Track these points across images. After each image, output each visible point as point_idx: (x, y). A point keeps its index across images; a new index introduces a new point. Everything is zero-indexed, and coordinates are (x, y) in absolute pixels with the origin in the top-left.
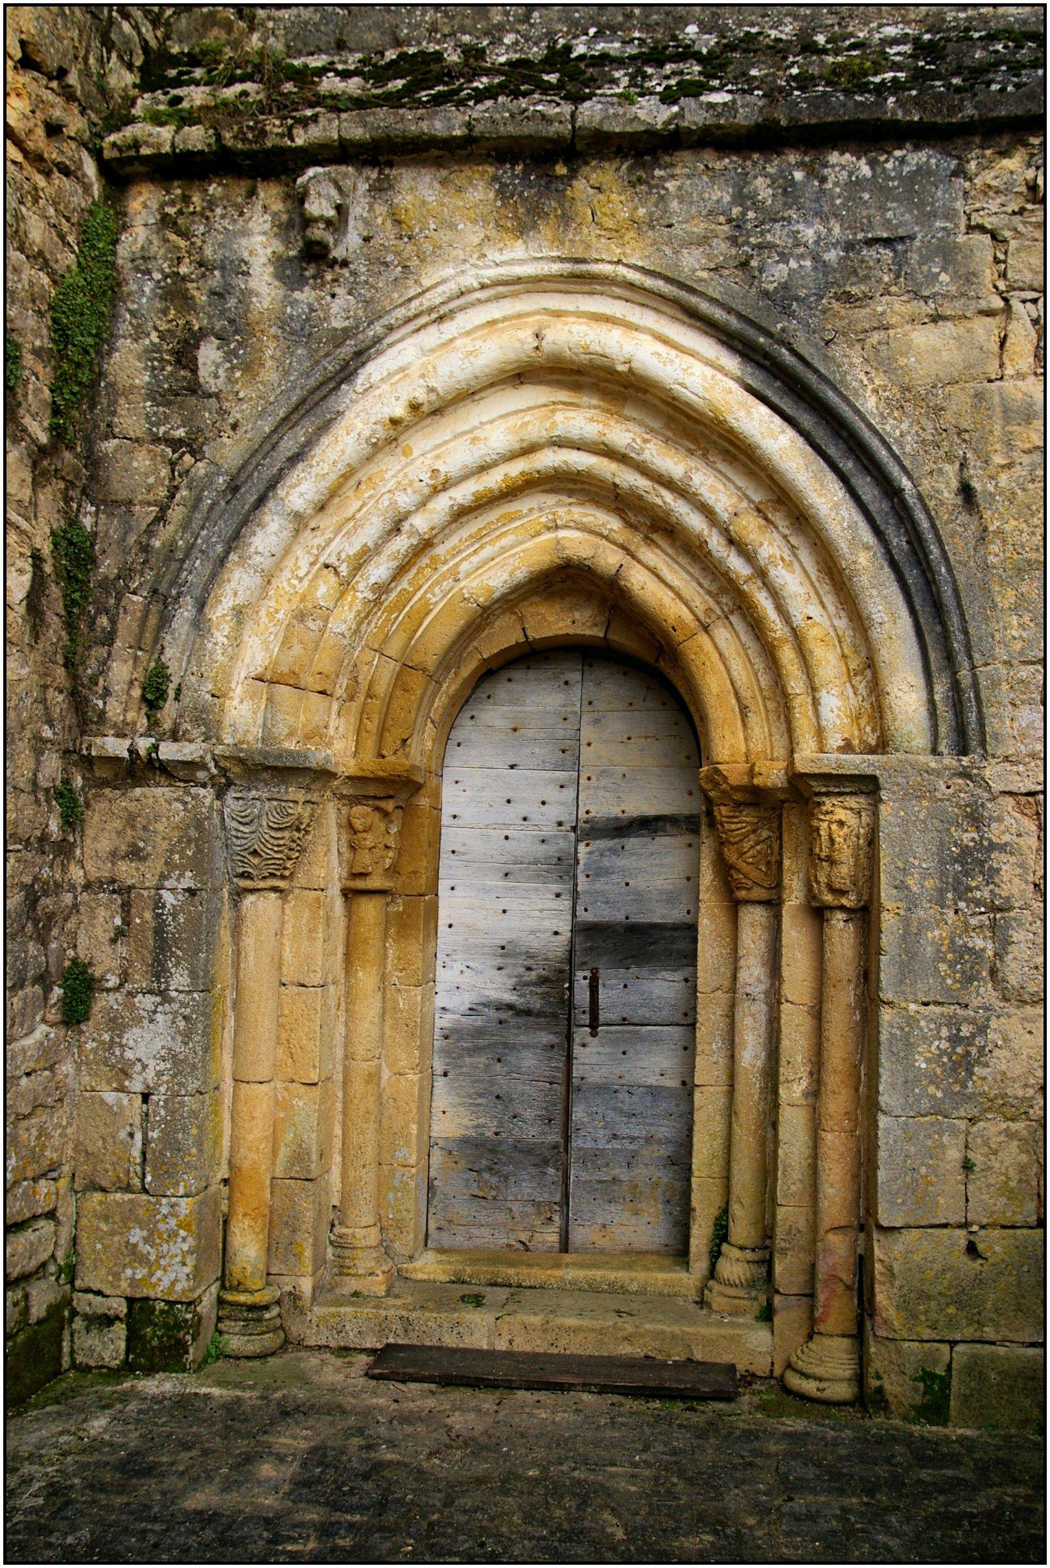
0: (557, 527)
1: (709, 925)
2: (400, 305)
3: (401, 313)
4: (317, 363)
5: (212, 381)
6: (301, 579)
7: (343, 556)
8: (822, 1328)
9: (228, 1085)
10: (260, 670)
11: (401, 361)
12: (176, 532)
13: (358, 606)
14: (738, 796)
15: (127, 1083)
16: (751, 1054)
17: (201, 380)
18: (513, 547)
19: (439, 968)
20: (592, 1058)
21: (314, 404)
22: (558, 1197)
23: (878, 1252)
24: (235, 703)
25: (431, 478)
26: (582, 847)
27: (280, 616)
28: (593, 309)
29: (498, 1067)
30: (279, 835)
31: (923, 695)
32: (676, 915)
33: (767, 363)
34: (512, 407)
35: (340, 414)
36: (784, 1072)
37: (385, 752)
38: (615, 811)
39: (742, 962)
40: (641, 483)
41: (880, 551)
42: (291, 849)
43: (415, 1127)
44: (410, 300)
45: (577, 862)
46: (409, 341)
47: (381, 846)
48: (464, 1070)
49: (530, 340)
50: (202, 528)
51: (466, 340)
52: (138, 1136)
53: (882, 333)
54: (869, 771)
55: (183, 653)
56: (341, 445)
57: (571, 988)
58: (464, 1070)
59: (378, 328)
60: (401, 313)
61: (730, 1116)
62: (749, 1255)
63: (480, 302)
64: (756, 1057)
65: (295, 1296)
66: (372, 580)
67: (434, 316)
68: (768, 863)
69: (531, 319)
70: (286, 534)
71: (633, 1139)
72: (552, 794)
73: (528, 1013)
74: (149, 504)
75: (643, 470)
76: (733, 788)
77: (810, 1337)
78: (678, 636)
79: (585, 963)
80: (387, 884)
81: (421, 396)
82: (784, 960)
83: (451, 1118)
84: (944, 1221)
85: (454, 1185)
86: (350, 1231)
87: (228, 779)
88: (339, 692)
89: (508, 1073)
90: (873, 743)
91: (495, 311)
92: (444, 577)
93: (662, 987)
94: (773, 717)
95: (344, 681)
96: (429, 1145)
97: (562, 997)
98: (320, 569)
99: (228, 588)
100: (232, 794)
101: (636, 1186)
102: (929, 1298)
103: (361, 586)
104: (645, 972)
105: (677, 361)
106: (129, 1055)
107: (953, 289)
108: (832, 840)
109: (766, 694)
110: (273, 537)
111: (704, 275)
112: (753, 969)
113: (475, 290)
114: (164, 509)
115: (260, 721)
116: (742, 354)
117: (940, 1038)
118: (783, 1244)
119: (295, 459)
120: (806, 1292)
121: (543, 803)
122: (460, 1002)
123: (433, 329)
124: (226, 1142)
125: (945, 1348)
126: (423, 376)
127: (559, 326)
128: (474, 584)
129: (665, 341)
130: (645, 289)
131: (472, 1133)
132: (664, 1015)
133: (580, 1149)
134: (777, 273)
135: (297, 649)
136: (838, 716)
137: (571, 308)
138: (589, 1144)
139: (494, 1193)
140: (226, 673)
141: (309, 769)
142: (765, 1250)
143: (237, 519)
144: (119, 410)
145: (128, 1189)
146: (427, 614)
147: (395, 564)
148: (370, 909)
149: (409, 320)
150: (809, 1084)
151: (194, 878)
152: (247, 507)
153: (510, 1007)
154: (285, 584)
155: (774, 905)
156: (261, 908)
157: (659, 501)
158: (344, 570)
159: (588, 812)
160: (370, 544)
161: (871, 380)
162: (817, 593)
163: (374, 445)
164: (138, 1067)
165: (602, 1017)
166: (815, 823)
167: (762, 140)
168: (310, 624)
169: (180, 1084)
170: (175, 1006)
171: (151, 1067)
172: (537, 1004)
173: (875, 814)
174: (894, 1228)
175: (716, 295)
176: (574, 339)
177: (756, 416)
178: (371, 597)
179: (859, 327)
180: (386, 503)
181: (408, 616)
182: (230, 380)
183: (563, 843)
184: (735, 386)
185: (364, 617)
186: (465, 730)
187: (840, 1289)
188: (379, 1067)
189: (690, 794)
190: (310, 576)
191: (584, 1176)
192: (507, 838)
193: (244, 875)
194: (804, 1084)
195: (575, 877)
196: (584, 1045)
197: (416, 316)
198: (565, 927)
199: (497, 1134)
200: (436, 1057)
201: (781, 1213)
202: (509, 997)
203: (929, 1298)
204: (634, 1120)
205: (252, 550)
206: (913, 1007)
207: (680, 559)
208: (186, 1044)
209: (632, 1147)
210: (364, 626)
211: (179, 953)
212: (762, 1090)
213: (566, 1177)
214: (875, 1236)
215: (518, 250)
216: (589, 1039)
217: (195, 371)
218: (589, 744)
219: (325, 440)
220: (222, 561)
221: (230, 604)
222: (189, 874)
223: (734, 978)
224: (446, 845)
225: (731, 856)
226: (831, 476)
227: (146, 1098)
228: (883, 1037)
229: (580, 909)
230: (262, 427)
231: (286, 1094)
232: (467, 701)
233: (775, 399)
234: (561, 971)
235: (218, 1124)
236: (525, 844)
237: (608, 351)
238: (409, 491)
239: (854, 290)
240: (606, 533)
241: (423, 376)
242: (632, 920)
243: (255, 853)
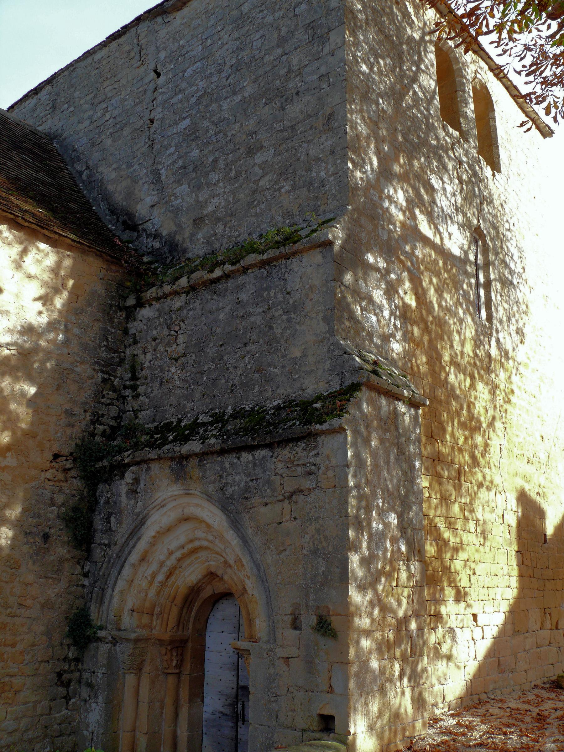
56: (142, 545)
59: (146, 512)
73: (226, 715)
100: (118, 645)
106: (90, 721)
111: (213, 493)
134: (230, 490)
153: (222, 712)
158: (149, 578)
167: (222, 452)
182: (117, 527)
198: (235, 687)
202: (221, 709)
215: (175, 487)
239: (247, 496)
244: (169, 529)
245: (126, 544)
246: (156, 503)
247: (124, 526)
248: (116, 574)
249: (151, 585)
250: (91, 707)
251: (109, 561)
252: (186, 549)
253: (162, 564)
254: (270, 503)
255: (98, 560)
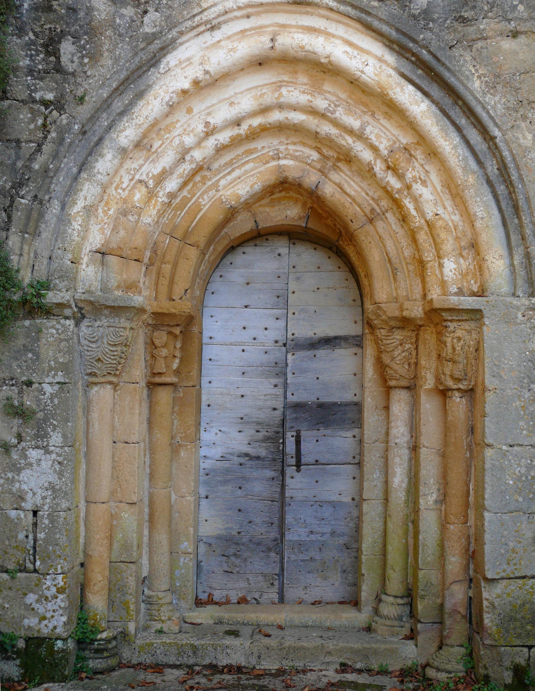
0: (279, 158)
1: (371, 401)
2: (189, 19)
3: (189, 23)
4: (136, 54)
5: (70, 64)
6: (124, 190)
7: (151, 175)
8: (448, 641)
9: (82, 505)
10: (99, 246)
11: (187, 55)
12: (48, 159)
13: (159, 207)
14: (393, 323)
15: (23, 504)
16: (399, 479)
17: (63, 64)
18: (252, 170)
19: (202, 432)
20: (297, 484)
21: (134, 80)
22: (277, 571)
23: (485, 595)
24: (84, 266)
25: (205, 127)
26: (289, 356)
27: (111, 212)
28: (306, 24)
29: (239, 492)
30: (114, 349)
31: (507, 261)
32: (348, 397)
33: (413, 59)
34: (255, 84)
35: (150, 87)
36: (422, 489)
37: (174, 298)
38: (310, 334)
39: (393, 424)
40: (333, 131)
41: (480, 172)
42: (121, 358)
43: (192, 529)
44: (194, 16)
45: (287, 365)
46: (192, 42)
47: (171, 356)
48: (218, 494)
49: (268, 42)
50: (65, 158)
51: (228, 42)
52: (31, 537)
53: (483, 42)
54: (477, 307)
55: (52, 235)
56: (151, 107)
57: (283, 443)
58: (218, 494)
59: (174, 33)
60: (189, 23)
61: (386, 518)
62: (400, 601)
63: (237, 18)
64: (402, 481)
65: (124, 634)
66: (168, 190)
67: (209, 26)
68: (409, 364)
69: (269, 29)
70: (116, 161)
71: (323, 534)
72: (271, 323)
73: (258, 458)
74: (31, 141)
75: (335, 123)
76: (389, 318)
77: (440, 648)
78: (354, 226)
79: (292, 427)
80: (174, 380)
81: (200, 75)
82: (422, 422)
83: (212, 523)
84: (523, 575)
85: (213, 563)
86: (155, 593)
87: (82, 314)
88: (146, 260)
89: (246, 495)
90: (476, 290)
91: (245, 24)
92: (209, 189)
93: (342, 441)
94: (412, 275)
95: (148, 254)
96: (198, 540)
97: (278, 448)
98: (136, 183)
99: (82, 194)
100: (85, 323)
101: (325, 563)
102: (516, 620)
103: (161, 194)
104: (328, 432)
105: (359, 57)
106: (24, 487)
107: (526, 15)
108: (454, 349)
109: (408, 261)
110: (109, 164)
112: (400, 428)
113: (234, 10)
114: (40, 146)
115: (99, 278)
116: (398, 53)
117: (521, 467)
118: (423, 593)
119: (122, 114)
120: (438, 620)
121: (266, 329)
122: (216, 452)
123: (207, 34)
124: (82, 540)
125: (526, 650)
126: (201, 64)
127: (286, 34)
128: (229, 193)
129: (350, 44)
130: (339, 13)
131: (223, 532)
132: (341, 458)
133: (290, 541)
135: (122, 233)
136: (455, 274)
137: (293, 23)
138: (296, 538)
139: (238, 569)
140: (79, 247)
141: (134, 307)
142: (410, 596)
143: (85, 152)
144: (10, 81)
145: (24, 570)
146: (199, 211)
147: (181, 180)
148: (164, 396)
149: (193, 28)
150: (438, 496)
151: (64, 376)
152: (92, 144)
153: (246, 455)
154: (114, 192)
155: (412, 388)
156: (102, 395)
157: (343, 142)
158: (151, 183)
159: (293, 334)
160: (167, 168)
161: (477, 71)
162: (442, 201)
163: (171, 106)
164: (30, 495)
165: (304, 460)
166: (444, 339)
168: (130, 217)
169: (57, 504)
170: (54, 456)
171: (39, 494)
172: (263, 453)
173: (480, 333)
174: (495, 579)
175: (383, 17)
176: (295, 43)
177: (406, 91)
178: (167, 201)
179: (469, 38)
180: (177, 142)
181: (187, 212)
182: (82, 64)
183: (278, 353)
184: (393, 73)
185: (161, 214)
186: (216, 284)
187: (459, 617)
188: (170, 492)
189: (356, 323)
190: (129, 188)
191: (293, 557)
192: (243, 351)
193: (94, 375)
194: (435, 496)
195: (285, 374)
196: (292, 478)
197: (198, 26)
198: (279, 404)
199: (239, 533)
200: (201, 486)
201: (421, 574)
203: (516, 620)
204: (323, 522)
205: (96, 171)
206: (504, 448)
207: (355, 178)
208: (60, 479)
209: (322, 539)
210: (161, 219)
211: (55, 422)
212: (406, 502)
213: (282, 558)
214: (483, 584)
216: (295, 474)
217: (58, 58)
218: (294, 293)
219: (141, 103)
220: (76, 178)
221: (83, 205)
222: (60, 373)
223: (387, 434)
224: (206, 355)
225: (386, 359)
226: (451, 128)
227: (35, 513)
228: (487, 466)
229: (289, 394)
230: (102, 93)
231: (117, 510)
232: (218, 266)
233: (418, 81)
234: (278, 433)
235: (78, 529)
236: (255, 354)
237: (316, 50)
238: (191, 135)
239: (466, 15)
240: (309, 162)
241: (201, 64)
242: (321, 400)
243: (99, 360)
244: (225, 77)
245: (106, 105)
246: (205, 17)
247: (107, 61)
248: (75, 170)
249: (150, 199)
250: (26, 457)
251: (61, 141)
252: (245, 126)
253: (183, 154)
254: (525, 33)
255: (24, 137)
